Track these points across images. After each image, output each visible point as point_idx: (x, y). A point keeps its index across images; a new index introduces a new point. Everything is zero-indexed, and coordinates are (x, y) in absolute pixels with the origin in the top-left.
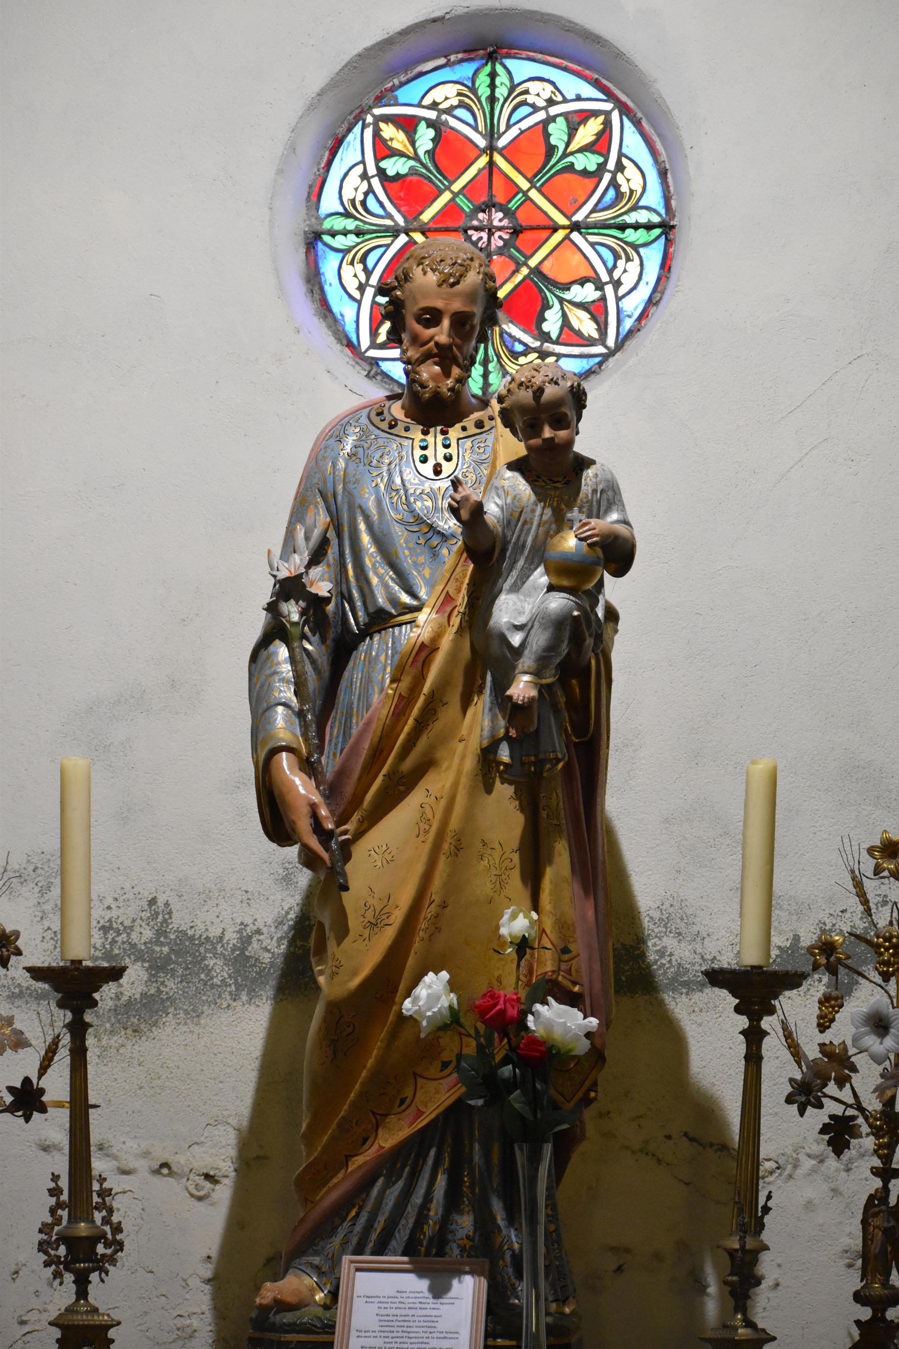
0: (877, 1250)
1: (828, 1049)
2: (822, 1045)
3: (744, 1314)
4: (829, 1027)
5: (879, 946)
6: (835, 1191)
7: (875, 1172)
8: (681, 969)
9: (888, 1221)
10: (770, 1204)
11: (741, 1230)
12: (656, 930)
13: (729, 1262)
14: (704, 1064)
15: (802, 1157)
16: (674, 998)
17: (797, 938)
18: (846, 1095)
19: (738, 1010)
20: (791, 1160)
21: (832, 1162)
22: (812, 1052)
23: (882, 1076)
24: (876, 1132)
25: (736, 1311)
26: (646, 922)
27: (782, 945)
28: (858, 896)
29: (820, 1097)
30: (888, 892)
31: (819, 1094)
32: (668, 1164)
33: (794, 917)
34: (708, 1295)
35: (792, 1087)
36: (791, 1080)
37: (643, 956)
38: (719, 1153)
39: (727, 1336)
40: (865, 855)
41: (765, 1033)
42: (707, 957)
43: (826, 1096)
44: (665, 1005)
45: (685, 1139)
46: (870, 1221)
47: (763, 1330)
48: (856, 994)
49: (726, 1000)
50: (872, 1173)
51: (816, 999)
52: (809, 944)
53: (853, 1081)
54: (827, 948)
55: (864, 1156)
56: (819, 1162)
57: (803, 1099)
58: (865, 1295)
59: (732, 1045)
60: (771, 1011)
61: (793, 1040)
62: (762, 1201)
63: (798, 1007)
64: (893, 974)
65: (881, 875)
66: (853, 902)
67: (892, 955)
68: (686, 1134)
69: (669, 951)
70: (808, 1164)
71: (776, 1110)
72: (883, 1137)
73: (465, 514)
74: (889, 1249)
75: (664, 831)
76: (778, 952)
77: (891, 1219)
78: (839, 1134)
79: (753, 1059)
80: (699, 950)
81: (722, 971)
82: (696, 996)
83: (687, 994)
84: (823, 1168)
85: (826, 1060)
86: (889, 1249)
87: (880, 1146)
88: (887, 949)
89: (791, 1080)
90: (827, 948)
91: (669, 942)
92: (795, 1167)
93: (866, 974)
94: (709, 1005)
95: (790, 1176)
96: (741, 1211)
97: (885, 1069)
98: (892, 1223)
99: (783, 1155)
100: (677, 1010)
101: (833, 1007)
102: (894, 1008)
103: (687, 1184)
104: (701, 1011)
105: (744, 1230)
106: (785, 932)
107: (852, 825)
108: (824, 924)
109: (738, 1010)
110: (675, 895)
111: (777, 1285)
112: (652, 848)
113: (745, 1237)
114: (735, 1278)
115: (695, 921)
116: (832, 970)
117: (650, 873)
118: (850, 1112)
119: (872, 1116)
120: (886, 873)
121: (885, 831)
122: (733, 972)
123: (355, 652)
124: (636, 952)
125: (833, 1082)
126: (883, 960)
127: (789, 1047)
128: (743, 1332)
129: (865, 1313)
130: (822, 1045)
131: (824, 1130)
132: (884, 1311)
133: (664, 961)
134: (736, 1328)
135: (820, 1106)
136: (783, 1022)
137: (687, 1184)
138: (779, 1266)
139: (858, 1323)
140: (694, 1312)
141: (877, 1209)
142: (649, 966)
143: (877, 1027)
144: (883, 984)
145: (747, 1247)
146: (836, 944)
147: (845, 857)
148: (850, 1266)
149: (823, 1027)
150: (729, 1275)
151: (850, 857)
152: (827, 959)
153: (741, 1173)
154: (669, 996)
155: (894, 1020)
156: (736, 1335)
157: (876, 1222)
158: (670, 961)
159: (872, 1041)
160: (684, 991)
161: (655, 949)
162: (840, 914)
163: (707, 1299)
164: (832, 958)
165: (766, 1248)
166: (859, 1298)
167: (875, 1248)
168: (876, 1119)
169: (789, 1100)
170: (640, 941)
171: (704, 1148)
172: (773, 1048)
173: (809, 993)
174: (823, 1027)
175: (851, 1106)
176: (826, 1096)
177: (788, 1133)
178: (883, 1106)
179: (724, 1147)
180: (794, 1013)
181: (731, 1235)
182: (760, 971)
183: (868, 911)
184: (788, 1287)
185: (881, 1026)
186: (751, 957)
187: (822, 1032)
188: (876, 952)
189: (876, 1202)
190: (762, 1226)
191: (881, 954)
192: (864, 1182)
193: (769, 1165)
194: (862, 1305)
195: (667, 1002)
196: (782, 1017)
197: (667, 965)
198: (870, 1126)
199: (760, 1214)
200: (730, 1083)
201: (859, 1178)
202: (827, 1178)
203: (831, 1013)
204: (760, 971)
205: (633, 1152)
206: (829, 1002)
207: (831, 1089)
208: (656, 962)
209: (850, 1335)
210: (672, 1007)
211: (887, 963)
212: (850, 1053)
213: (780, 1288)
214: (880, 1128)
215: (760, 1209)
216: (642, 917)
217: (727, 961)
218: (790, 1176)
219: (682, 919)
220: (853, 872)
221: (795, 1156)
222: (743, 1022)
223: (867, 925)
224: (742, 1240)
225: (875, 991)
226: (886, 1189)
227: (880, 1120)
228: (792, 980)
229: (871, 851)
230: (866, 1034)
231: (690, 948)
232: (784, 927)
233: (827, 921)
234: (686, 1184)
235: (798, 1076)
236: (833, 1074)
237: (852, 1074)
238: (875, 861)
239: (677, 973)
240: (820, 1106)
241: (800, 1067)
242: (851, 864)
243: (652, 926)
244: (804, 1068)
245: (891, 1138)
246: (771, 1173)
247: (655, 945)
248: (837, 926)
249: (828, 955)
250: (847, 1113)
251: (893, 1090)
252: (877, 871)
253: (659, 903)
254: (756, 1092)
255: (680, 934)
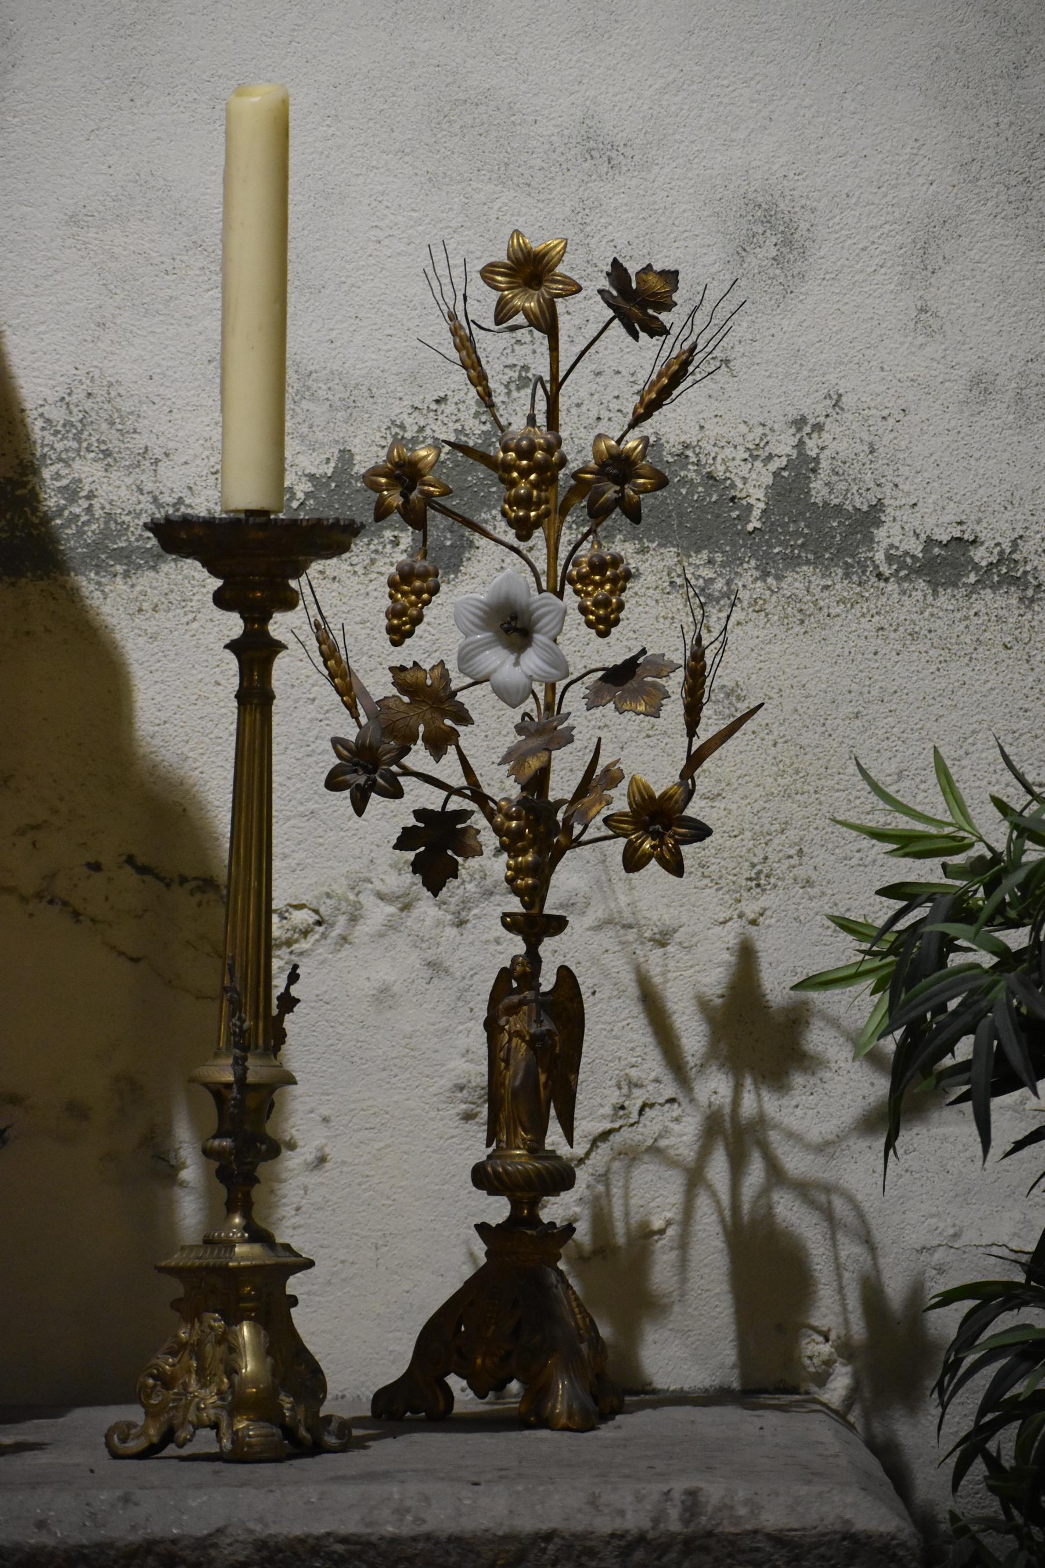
0: (518, 1082)
1: (409, 677)
2: (398, 671)
3: (247, 1215)
4: (410, 634)
5: (506, 467)
6: (435, 967)
7: (510, 922)
8: (113, 526)
9: (540, 1022)
10: (295, 991)
11: (236, 1045)
12: (59, 446)
13: (214, 1112)
14: (163, 716)
15: (368, 900)
16: (99, 583)
17: (346, 457)
18: (449, 770)
19: (221, 600)
20: (344, 906)
21: (428, 909)
22: (379, 686)
23: (520, 729)
24: (510, 844)
25: (231, 1207)
26: (37, 429)
27: (318, 472)
28: (464, 367)
29: (395, 775)
30: (529, 360)
31: (394, 768)
32: (93, 920)
33: (341, 415)
34: (182, 1184)
35: (339, 755)
36: (336, 742)
37: (33, 499)
38: (198, 897)
39: (211, 1262)
40: (478, 288)
41: (278, 647)
42: (166, 499)
43: (407, 772)
44: (81, 599)
45: (128, 869)
46: (502, 1021)
47: (287, 1247)
48: (469, 568)
49: (196, 580)
50: (505, 924)
51: (384, 580)
52: (370, 465)
53: (462, 742)
54: (404, 473)
55: (491, 894)
56: (402, 910)
57: (362, 779)
58: (495, 1171)
59: (219, 677)
60: (289, 602)
61: (339, 661)
62: (279, 984)
63: (345, 592)
64: (537, 524)
65: (511, 323)
66: (456, 381)
67: (535, 485)
68: (130, 860)
69: (87, 488)
70: (378, 913)
71: (312, 806)
72: (524, 852)
73: (1010, 812)
74: (543, 1078)
75: (69, 242)
76: (308, 487)
77: (543, 1016)
78: (435, 848)
79: (255, 699)
80: (149, 486)
81: (187, 522)
82: (146, 579)
83: (126, 575)
84: (411, 920)
85: (406, 699)
86: (543, 1078)
87: (518, 871)
88: (524, 473)
89: (336, 742)
90: (404, 473)
91: (87, 471)
92: (354, 919)
93: (489, 528)
94: (171, 597)
95: (344, 939)
96: (236, 1007)
97: (525, 714)
98: (547, 1025)
99: (328, 895)
100: (106, 609)
101: (418, 593)
102: (540, 590)
103: (135, 960)
104: (155, 609)
105: (242, 1045)
106: (323, 444)
107: (454, 224)
108: (402, 427)
109: (221, 600)
110: (96, 373)
111: (322, 1160)
112: (46, 278)
113: (245, 1059)
114: (226, 1143)
115: (139, 426)
116: (415, 519)
117: (43, 328)
118: (456, 803)
119: (500, 810)
120: (520, 319)
121: (517, 232)
122: (209, 523)
123: (4, 340)
124: (19, 492)
125: (420, 742)
126: (517, 495)
127: (332, 676)
128: (245, 1252)
129: (497, 1210)
130: (398, 671)
131: (406, 840)
132: (534, 1204)
133: (77, 510)
134: (230, 1245)
135: (396, 792)
136: (317, 626)
137: (135, 960)
138: (326, 1120)
139: (482, 1229)
140: (155, 1219)
141: (515, 999)
142: (46, 520)
143: (507, 631)
144: (516, 543)
145: (251, 1078)
146: (421, 465)
147: (437, 290)
148: (468, 1117)
149: (398, 635)
150: (214, 1137)
151: (448, 289)
152: (402, 495)
153: (234, 931)
154: (89, 580)
155: (538, 609)
156: (231, 1259)
157: (515, 1023)
158: (89, 510)
159: (497, 661)
160: (119, 568)
161: (58, 484)
162: (434, 406)
163: (180, 1192)
164: (415, 495)
165: (292, 1081)
166: (483, 1178)
167: (514, 1077)
168: (509, 817)
169: (333, 783)
170: (27, 469)
171: (168, 885)
172: (296, 674)
173: (374, 568)
174: (398, 635)
175: (458, 792)
176: (407, 772)
177: (329, 852)
178: (523, 789)
179: (208, 883)
180: (345, 608)
181: (217, 1055)
182: (263, 519)
183: (486, 398)
184: (343, 1163)
185: (516, 630)
186: (246, 493)
187: (396, 643)
188: (502, 480)
189: (515, 985)
190: (281, 1036)
191: (512, 484)
192: (493, 947)
193: (302, 918)
194: (490, 1193)
195: (85, 592)
196: (313, 611)
197: (84, 518)
198: (498, 830)
199: (275, 1011)
200: (218, 753)
201: (486, 937)
202: (419, 941)
203: (413, 605)
204: (263, 519)
205: (24, 899)
206: (409, 584)
207: (418, 758)
208: (61, 510)
209: (471, 1255)
210: (96, 603)
211: (525, 502)
212: (454, 686)
213: (328, 1165)
214: (518, 834)
215: (275, 1002)
216: (29, 420)
217: (204, 504)
218: (344, 939)
219: (112, 424)
220: (452, 317)
221: (352, 897)
222: (234, 625)
223: (488, 427)
224: (240, 1063)
225: (508, 561)
226: (533, 958)
227: (518, 818)
228: (330, 538)
229: (488, 273)
230: (487, 645)
231: (128, 481)
232: (320, 435)
233: (409, 421)
234: (132, 959)
235: (351, 733)
236: (421, 729)
237: (460, 729)
238: (495, 295)
239: (106, 534)
240: (396, 792)
241: (355, 716)
242: (451, 304)
243: (49, 439)
244: (364, 720)
245: (539, 853)
246: (305, 933)
247: (57, 476)
248: (428, 432)
249: (405, 488)
250: (451, 807)
251: (544, 756)
252: (502, 314)
253: (62, 391)
254: (261, 766)
255: (107, 453)
